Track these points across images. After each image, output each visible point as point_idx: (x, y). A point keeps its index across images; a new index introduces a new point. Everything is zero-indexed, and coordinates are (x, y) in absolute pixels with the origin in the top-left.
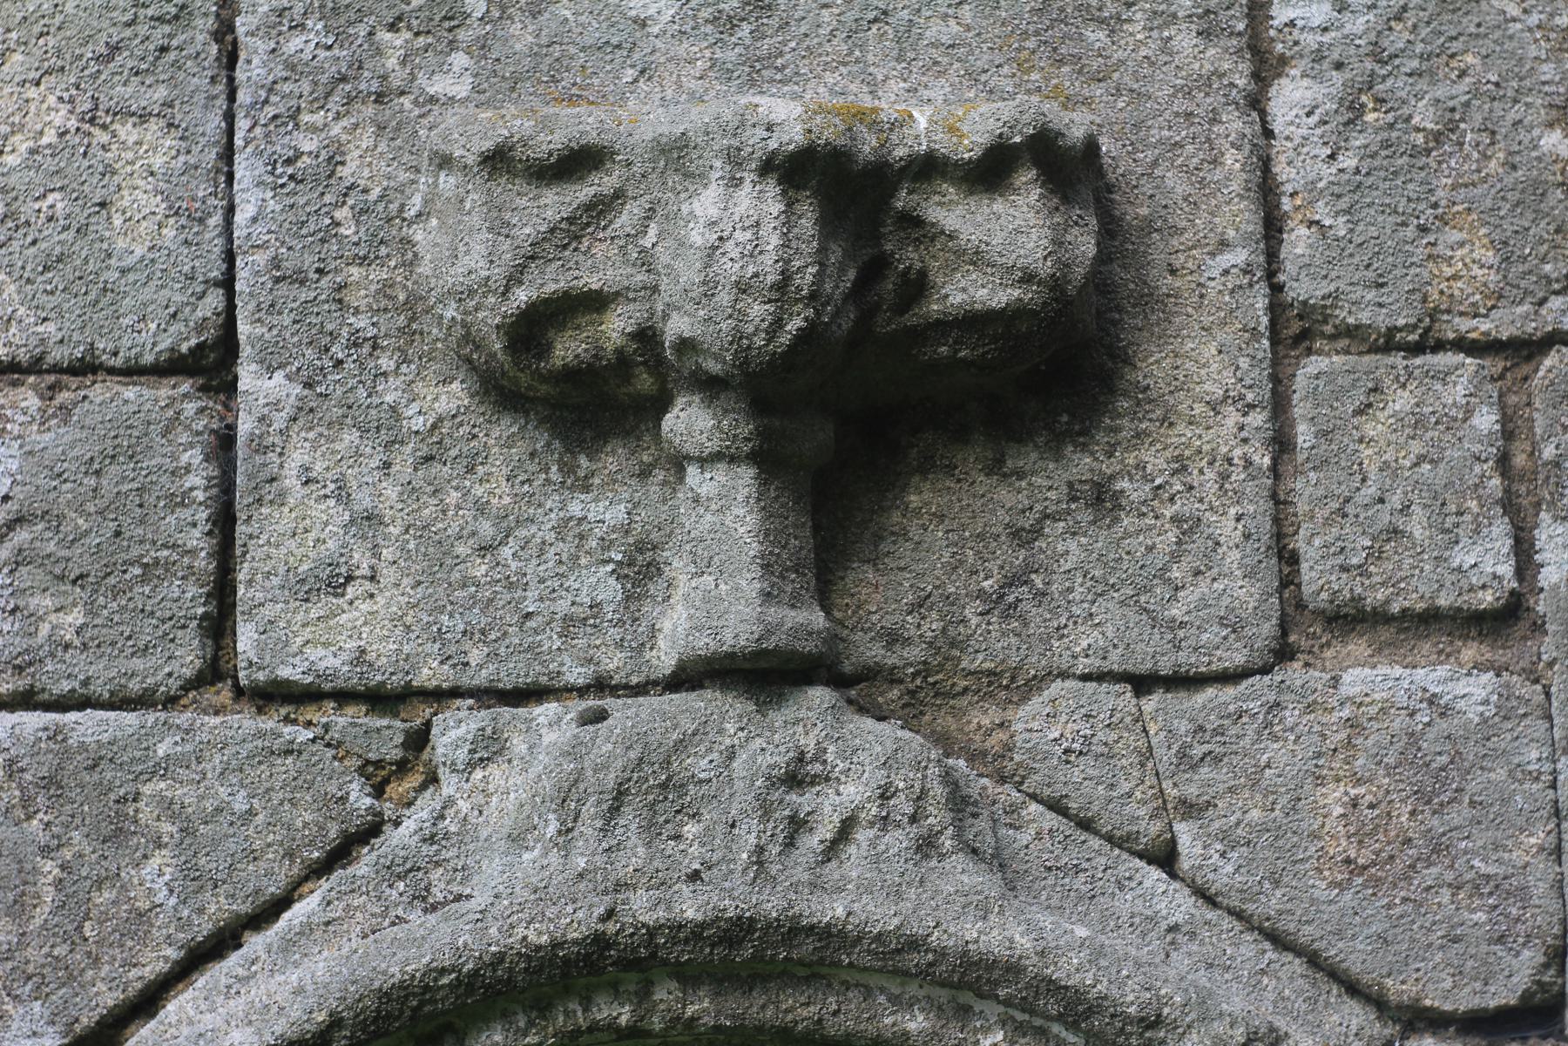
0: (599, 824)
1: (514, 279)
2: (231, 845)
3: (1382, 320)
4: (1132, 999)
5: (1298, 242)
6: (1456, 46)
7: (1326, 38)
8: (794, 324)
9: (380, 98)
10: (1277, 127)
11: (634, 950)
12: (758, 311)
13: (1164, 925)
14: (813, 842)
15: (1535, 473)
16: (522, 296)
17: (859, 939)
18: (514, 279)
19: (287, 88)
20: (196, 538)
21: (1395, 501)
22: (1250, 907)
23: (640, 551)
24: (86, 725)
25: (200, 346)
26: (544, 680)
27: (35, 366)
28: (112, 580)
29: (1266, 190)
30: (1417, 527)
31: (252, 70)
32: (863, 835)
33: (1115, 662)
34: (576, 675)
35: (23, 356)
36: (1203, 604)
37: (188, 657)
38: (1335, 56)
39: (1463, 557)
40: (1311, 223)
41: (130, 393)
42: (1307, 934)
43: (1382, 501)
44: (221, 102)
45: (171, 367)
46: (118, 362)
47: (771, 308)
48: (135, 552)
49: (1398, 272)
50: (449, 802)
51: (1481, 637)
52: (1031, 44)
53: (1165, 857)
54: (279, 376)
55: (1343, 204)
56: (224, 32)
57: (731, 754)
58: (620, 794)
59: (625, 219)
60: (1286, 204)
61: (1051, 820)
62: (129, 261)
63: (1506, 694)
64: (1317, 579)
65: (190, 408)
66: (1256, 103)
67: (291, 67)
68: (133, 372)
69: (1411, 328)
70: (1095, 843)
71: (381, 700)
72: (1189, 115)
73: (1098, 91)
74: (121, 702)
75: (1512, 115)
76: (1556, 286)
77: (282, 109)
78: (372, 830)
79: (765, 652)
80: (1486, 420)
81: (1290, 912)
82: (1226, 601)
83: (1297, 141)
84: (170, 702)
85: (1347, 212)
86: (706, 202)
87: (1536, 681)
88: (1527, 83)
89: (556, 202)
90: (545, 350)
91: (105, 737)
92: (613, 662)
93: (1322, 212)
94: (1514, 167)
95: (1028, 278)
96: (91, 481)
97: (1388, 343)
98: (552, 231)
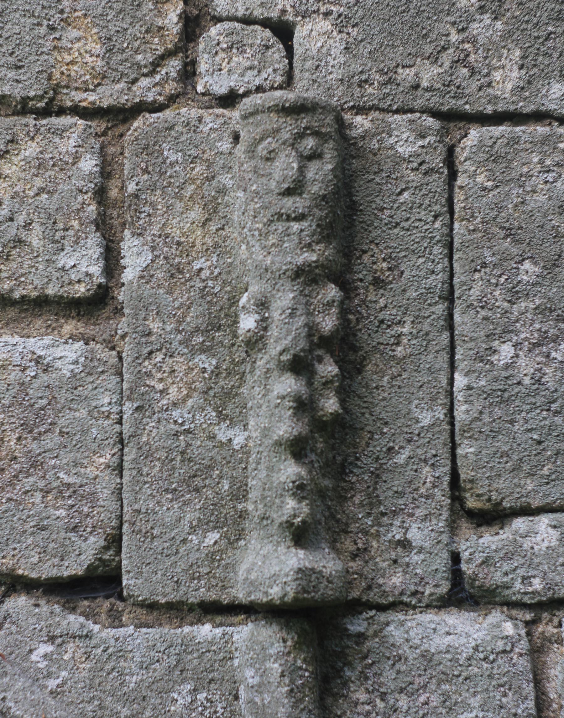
15: (123, 202)
21: (21, 219)
43: (11, 219)
49: (32, 58)
63: (91, 358)
76: (145, 71)
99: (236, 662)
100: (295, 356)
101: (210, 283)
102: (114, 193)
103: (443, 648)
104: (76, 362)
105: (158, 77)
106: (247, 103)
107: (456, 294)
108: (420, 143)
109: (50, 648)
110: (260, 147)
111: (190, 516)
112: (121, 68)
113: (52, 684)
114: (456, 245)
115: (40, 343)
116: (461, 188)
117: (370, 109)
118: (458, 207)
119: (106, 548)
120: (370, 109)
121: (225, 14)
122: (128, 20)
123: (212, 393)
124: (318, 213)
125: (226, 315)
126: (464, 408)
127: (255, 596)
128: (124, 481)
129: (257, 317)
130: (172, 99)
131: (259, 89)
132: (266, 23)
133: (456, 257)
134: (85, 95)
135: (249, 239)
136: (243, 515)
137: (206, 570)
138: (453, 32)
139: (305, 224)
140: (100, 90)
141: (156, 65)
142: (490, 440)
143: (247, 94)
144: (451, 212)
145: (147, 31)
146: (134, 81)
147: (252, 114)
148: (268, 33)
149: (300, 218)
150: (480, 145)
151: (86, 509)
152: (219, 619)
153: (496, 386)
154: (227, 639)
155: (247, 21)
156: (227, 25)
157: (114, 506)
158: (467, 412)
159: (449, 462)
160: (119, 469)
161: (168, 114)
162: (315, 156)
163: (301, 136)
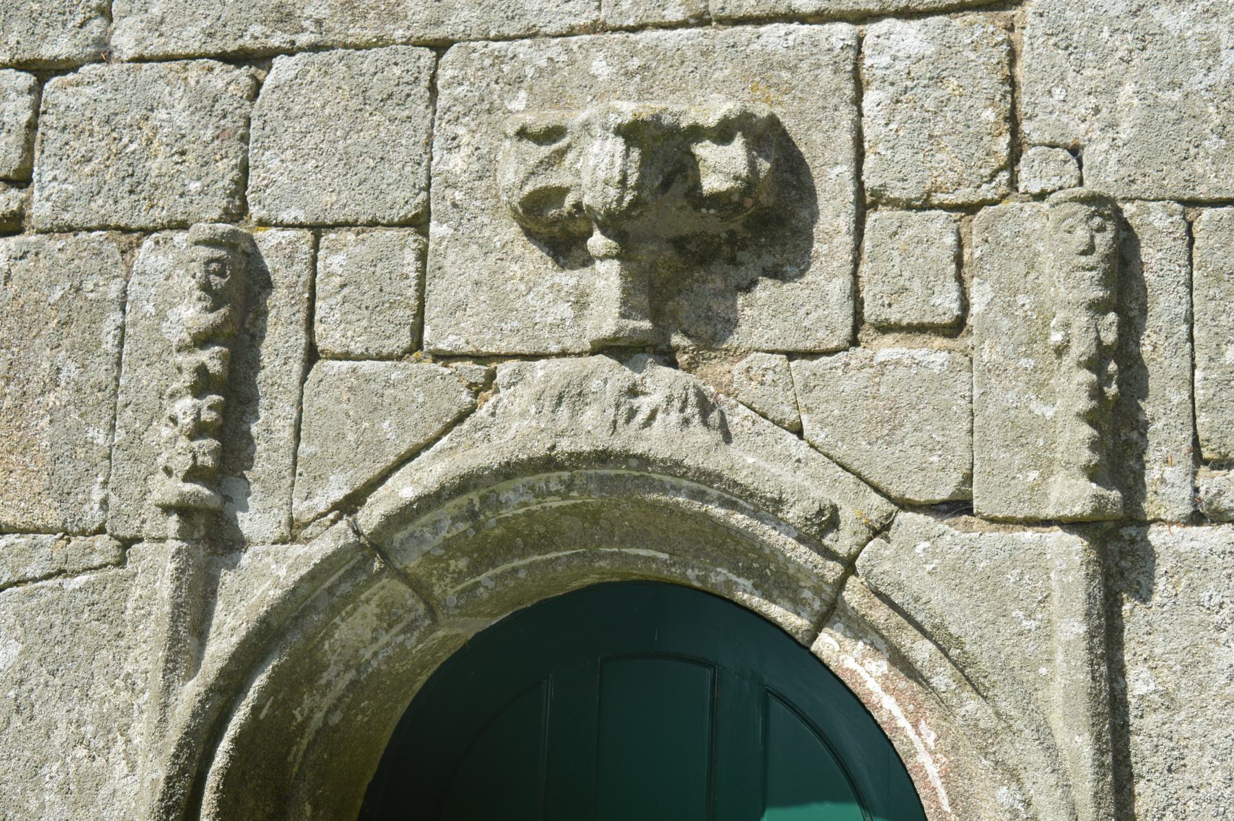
0: (551, 409)
1: (524, 183)
2: (416, 415)
3: (904, 195)
4: (770, 491)
5: (869, 162)
6: (945, 74)
7: (887, 72)
8: (628, 198)
9: (489, 111)
10: (865, 112)
11: (564, 462)
12: (613, 192)
13: (794, 459)
14: (640, 417)
15: (972, 263)
16: (528, 189)
17: (655, 461)
18: (524, 183)
19: (454, 109)
20: (411, 292)
21: (907, 274)
22: (832, 453)
23: (582, 297)
24: (367, 366)
25: (416, 215)
26: (541, 350)
27: (354, 224)
28: (378, 309)
29: (859, 140)
30: (916, 285)
31: (442, 102)
32: (659, 416)
33: (779, 346)
34: (554, 348)
35: (351, 219)
36: (819, 320)
37: (405, 340)
38: (890, 80)
39: (937, 300)
40: (876, 154)
41: (388, 233)
42: (855, 465)
43: (901, 275)
44: (430, 116)
45: (403, 224)
46: (385, 222)
47: (618, 191)
48: (386, 298)
49: (913, 174)
50: (501, 399)
51: (945, 336)
52: (758, 79)
53: (799, 433)
54: (445, 226)
55: (890, 145)
56: (433, 89)
57: (606, 381)
58: (560, 398)
59: (570, 156)
60: (866, 145)
61: (748, 412)
62: (391, 181)
64: (869, 311)
65: (411, 238)
66: (857, 100)
67: (456, 100)
68: (390, 225)
69: (917, 199)
70: (767, 423)
71: (479, 358)
72: (824, 108)
73: (786, 98)
74: (380, 358)
75: (969, 103)
76: (985, 179)
77: (452, 117)
78: (473, 409)
79: (618, 339)
80: (950, 240)
81: (849, 455)
82: (828, 319)
83: (872, 117)
84: (400, 358)
85: (893, 148)
86: (595, 147)
87: (966, 356)
88: (976, 89)
89: (545, 150)
90: (541, 212)
91: (373, 371)
92: (568, 343)
93: (881, 148)
94: (969, 127)
95: (736, 178)
96: (372, 269)
97: (908, 206)
98: (541, 162)
99: (1048, 556)
100: (1089, 358)
101: (1029, 313)
102: (966, 257)
103: (1188, 549)
104: (942, 365)
105: (994, 184)
106: (1053, 198)
107: (1196, 317)
108: (1170, 220)
109: (927, 544)
110: (1064, 224)
111: (1017, 460)
112: (970, 178)
113: (929, 567)
114: (1195, 285)
115: (920, 353)
116: (1197, 248)
117: (1135, 199)
118: (1196, 261)
119: (963, 483)
120: (1135, 199)
121: (1037, 142)
122: (974, 148)
123: (1032, 383)
124: (1103, 265)
125: (1041, 334)
126: (1201, 392)
127: (457, 529)
128: (975, 440)
129: (1063, 333)
130: (1004, 197)
131: (1061, 188)
132: (1065, 147)
133: (1194, 294)
134: (946, 196)
135: (1057, 284)
136: (1051, 462)
137: (1026, 497)
138: (1191, 147)
139: (1094, 273)
140: (956, 192)
141: (993, 176)
142: (1220, 414)
143: (1054, 191)
144: (1191, 264)
145: (987, 155)
146: (979, 187)
147: (1057, 204)
148: (1066, 152)
149: (1092, 269)
150: (1211, 220)
151: (950, 458)
152: (1040, 529)
153: (1223, 377)
154: (1040, 543)
155: (1053, 146)
156: (1040, 149)
157: (967, 456)
158: (1204, 395)
159: (1191, 428)
160: (971, 432)
161: (1001, 206)
162: (1101, 229)
163: (1092, 216)
